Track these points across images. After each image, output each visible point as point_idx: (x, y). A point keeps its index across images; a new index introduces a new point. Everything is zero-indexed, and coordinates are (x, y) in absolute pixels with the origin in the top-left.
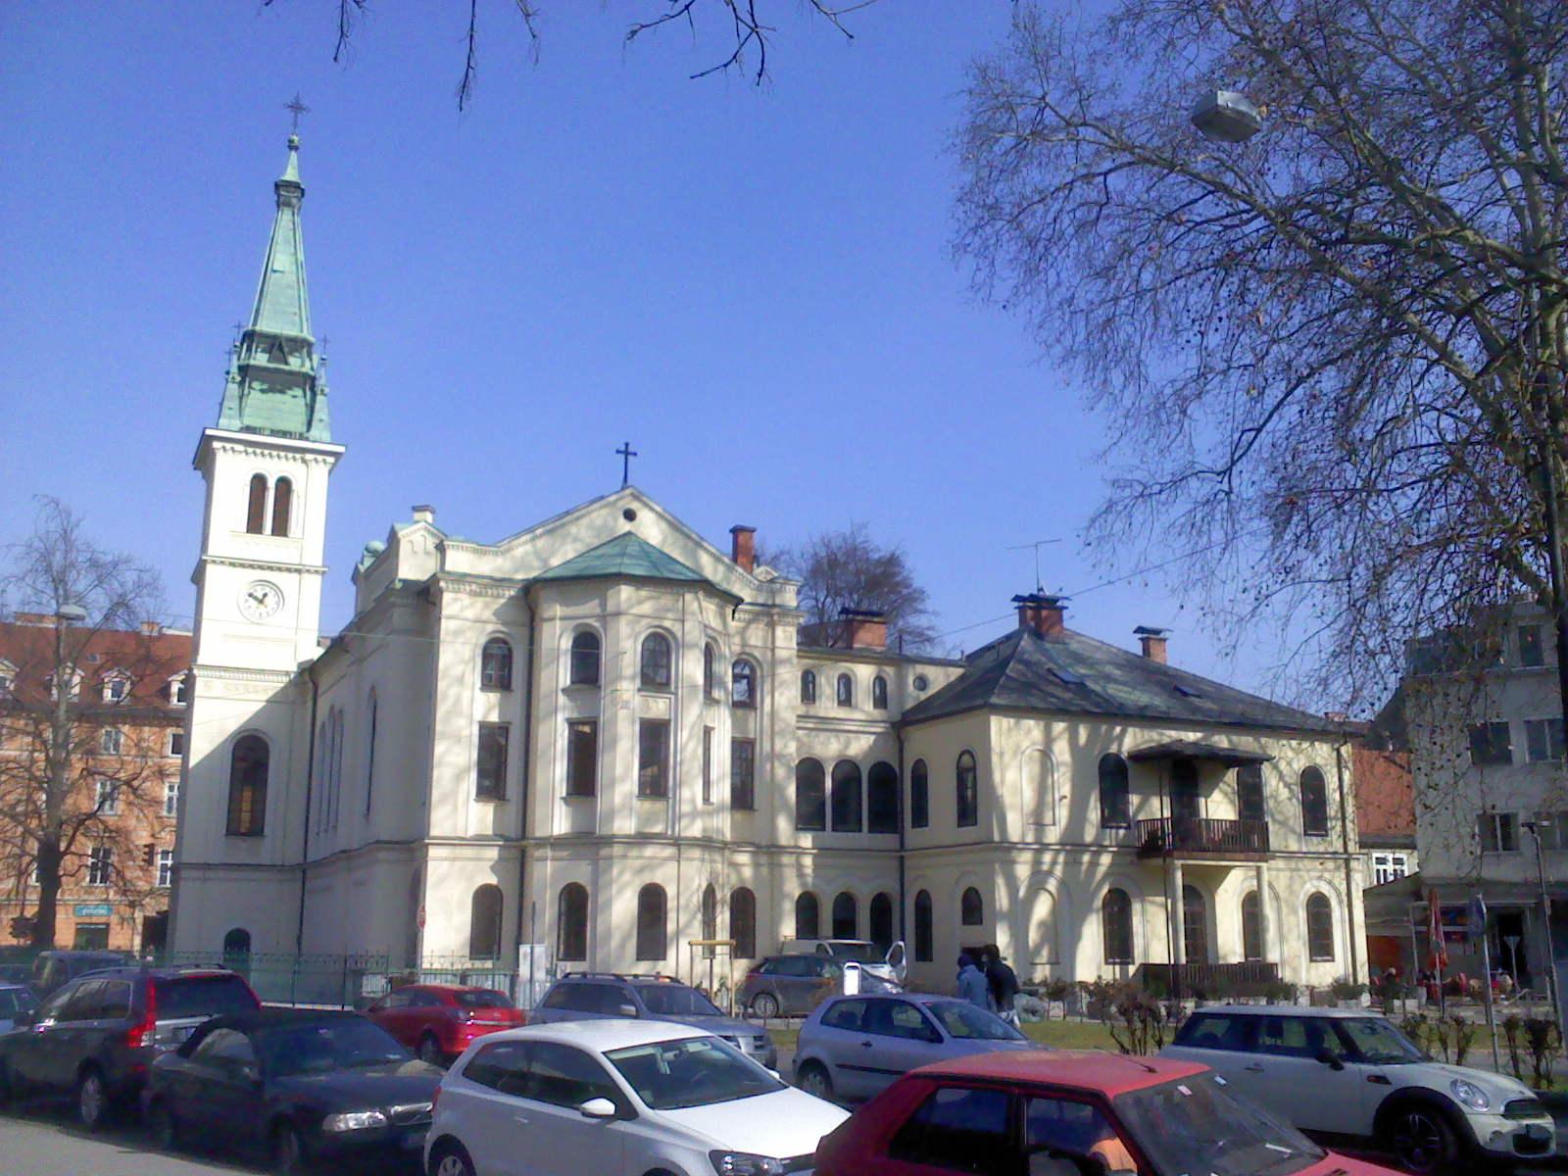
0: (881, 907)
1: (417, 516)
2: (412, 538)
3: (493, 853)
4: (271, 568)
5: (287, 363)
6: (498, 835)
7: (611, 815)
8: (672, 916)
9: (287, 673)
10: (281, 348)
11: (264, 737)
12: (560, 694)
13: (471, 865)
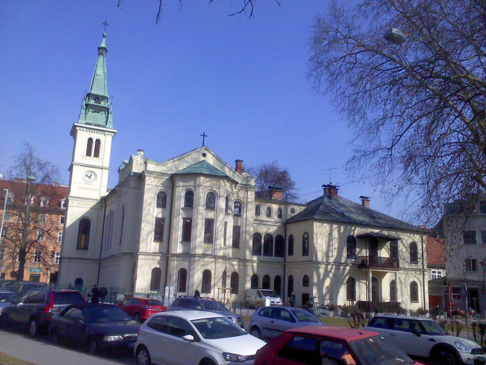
0: (278, 280)
1: (139, 153)
3: (158, 258)
4: (93, 167)
5: (100, 104)
8: (213, 280)
9: (97, 200)
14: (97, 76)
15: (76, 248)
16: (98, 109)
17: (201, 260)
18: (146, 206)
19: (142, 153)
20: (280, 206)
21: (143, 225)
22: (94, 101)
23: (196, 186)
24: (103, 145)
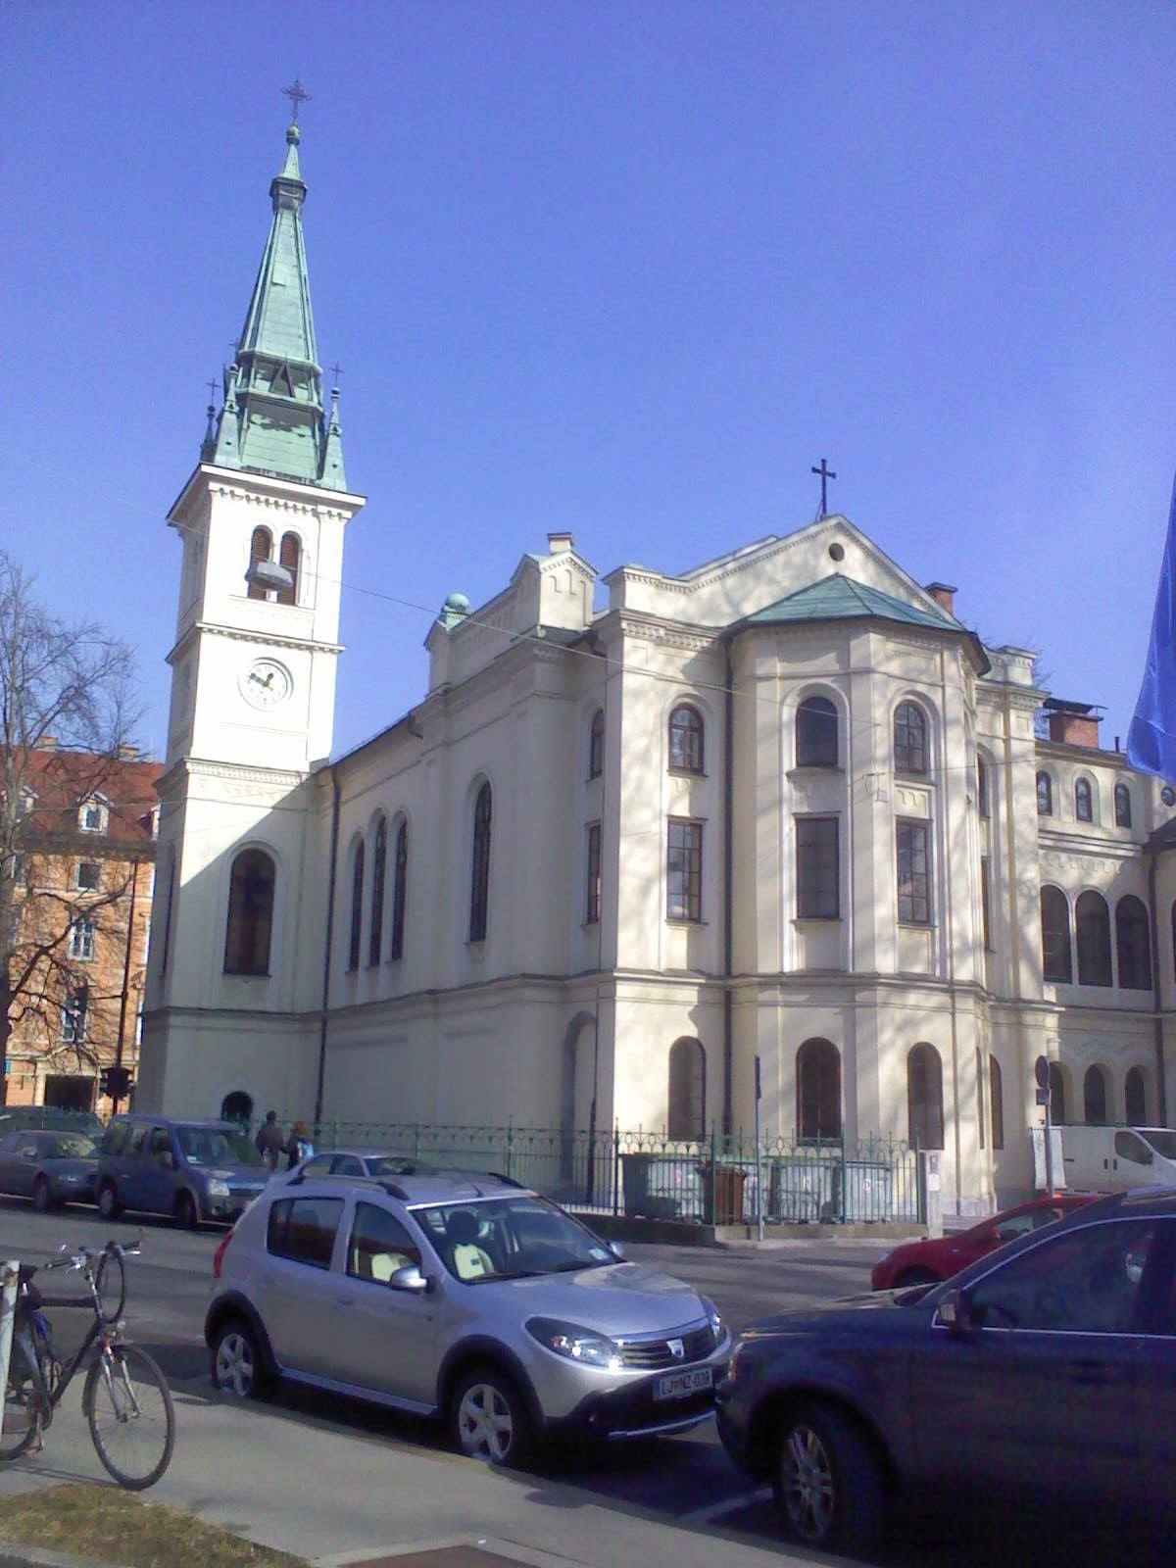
0: (1096, 1077)
1: (555, 546)
2: (553, 572)
3: (690, 995)
4: (277, 643)
6: (695, 970)
7: (870, 944)
8: (947, 1091)
9: (298, 774)
10: (285, 376)
11: (261, 847)
12: (785, 778)
13: (658, 1010)
14: (274, 289)
15: (221, 969)
16: (285, 417)
17: (896, 999)
18: (630, 766)
19: (567, 545)
20: (1119, 775)
21: (624, 847)
22: (268, 384)
23: (850, 675)
24: (313, 555)
